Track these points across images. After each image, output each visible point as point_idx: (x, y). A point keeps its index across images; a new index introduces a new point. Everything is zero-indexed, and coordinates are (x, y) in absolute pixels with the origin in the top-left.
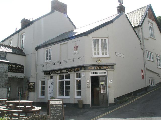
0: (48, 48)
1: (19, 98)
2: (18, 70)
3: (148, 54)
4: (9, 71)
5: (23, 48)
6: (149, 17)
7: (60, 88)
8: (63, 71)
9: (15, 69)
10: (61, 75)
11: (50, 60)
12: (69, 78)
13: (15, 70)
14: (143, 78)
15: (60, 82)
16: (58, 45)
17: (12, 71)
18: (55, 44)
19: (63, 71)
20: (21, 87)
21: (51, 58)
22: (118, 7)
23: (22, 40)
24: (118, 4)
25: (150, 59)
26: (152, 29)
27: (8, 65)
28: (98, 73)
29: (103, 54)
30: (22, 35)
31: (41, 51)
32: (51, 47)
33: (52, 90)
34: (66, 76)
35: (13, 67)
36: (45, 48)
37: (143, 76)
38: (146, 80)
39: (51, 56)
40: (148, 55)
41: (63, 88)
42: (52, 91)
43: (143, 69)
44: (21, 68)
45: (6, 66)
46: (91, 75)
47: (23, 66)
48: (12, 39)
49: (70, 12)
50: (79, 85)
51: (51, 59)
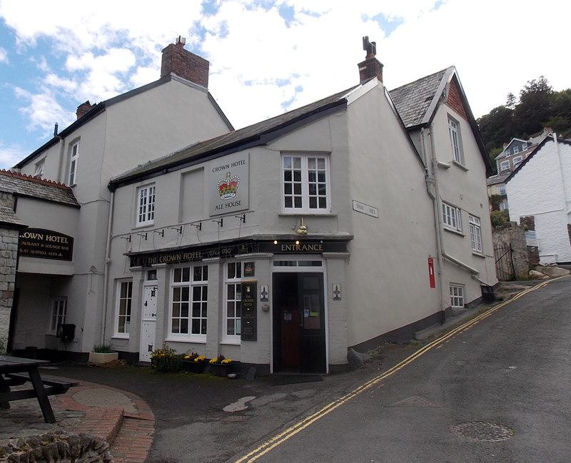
0: (147, 185)
1: (520, 139)
2: (54, 250)
3: (446, 209)
4: (19, 254)
5: (74, 183)
6: (450, 104)
7: (176, 307)
9: (42, 245)
10: (182, 266)
11: (151, 222)
12: (206, 278)
13: (43, 249)
14: (433, 285)
15: (176, 290)
16: (175, 176)
18: (167, 172)
19: (54, 239)
20: (62, 302)
21: (153, 216)
22: (360, 65)
23: (74, 163)
25: (451, 228)
26: (456, 137)
29: (313, 205)
30: (74, 145)
31: (126, 192)
33: (153, 315)
34: (197, 270)
35: (36, 241)
36: (138, 184)
37: (432, 278)
38: (441, 291)
39: (153, 210)
40: (447, 216)
41: (185, 307)
42: (154, 319)
43: (433, 255)
44: (64, 245)
46: (274, 271)
47: (71, 240)
49: (215, 85)
51: (153, 218)
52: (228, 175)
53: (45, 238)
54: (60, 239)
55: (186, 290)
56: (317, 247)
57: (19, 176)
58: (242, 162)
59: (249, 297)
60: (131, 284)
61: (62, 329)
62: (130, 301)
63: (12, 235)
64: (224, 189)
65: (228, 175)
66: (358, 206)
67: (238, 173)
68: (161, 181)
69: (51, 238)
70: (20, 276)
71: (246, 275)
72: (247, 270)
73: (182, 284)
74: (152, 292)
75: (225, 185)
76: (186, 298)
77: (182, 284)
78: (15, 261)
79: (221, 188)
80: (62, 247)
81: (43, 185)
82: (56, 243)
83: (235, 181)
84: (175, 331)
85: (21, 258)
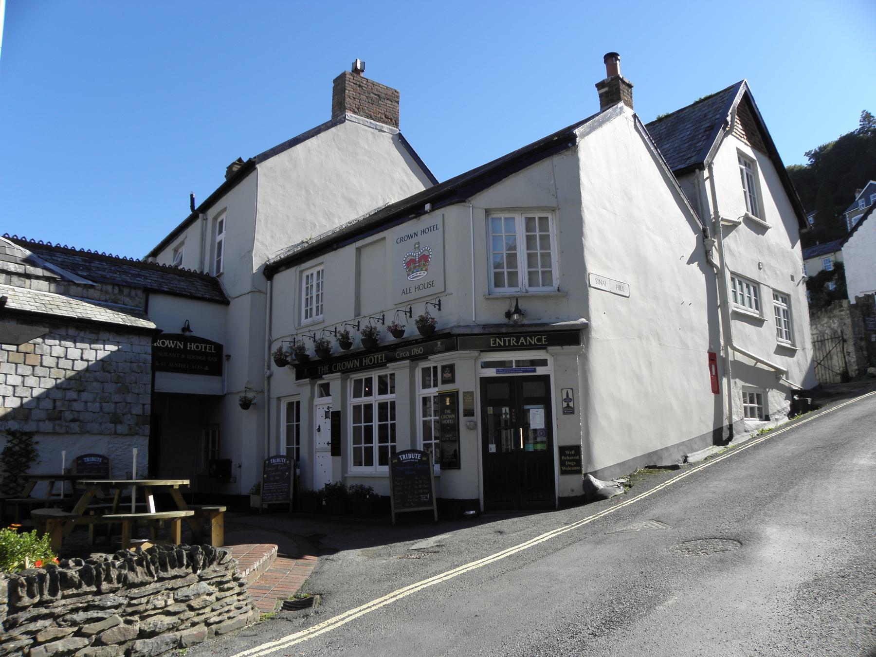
4: (154, 369)
5: (221, 271)
8: (371, 362)
9: (183, 356)
16: (348, 252)
17: (171, 365)
19: (197, 347)
23: (220, 243)
24: (602, 74)
27: (150, 340)
28: (192, 597)
30: (219, 220)
31: (286, 278)
32: (322, 263)
34: (382, 380)
35: (174, 350)
45: (144, 347)
47: (219, 347)
48: (182, 243)
50: (389, 444)
52: (417, 246)
53: (185, 346)
54: (205, 348)
55: (369, 407)
56: (539, 340)
57: (155, 267)
58: (434, 228)
59: (449, 411)
60: (298, 403)
61: (214, 467)
62: (298, 426)
63: (143, 343)
64: (412, 266)
65: (417, 246)
66: (598, 281)
67: (430, 243)
68: (330, 259)
69: (193, 347)
70: (159, 399)
71: (444, 382)
72: (445, 375)
73: (363, 400)
74: (326, 412)
75: (413, 261)
76: (369, 418)
77: (363, 400)
78: (150, 376)
79: (408, 264)
80: (209, 358)
81: (180, 276)
82: (200, 353)
83: (426, 253)
84: (358, 463)
85: (157, 374)
